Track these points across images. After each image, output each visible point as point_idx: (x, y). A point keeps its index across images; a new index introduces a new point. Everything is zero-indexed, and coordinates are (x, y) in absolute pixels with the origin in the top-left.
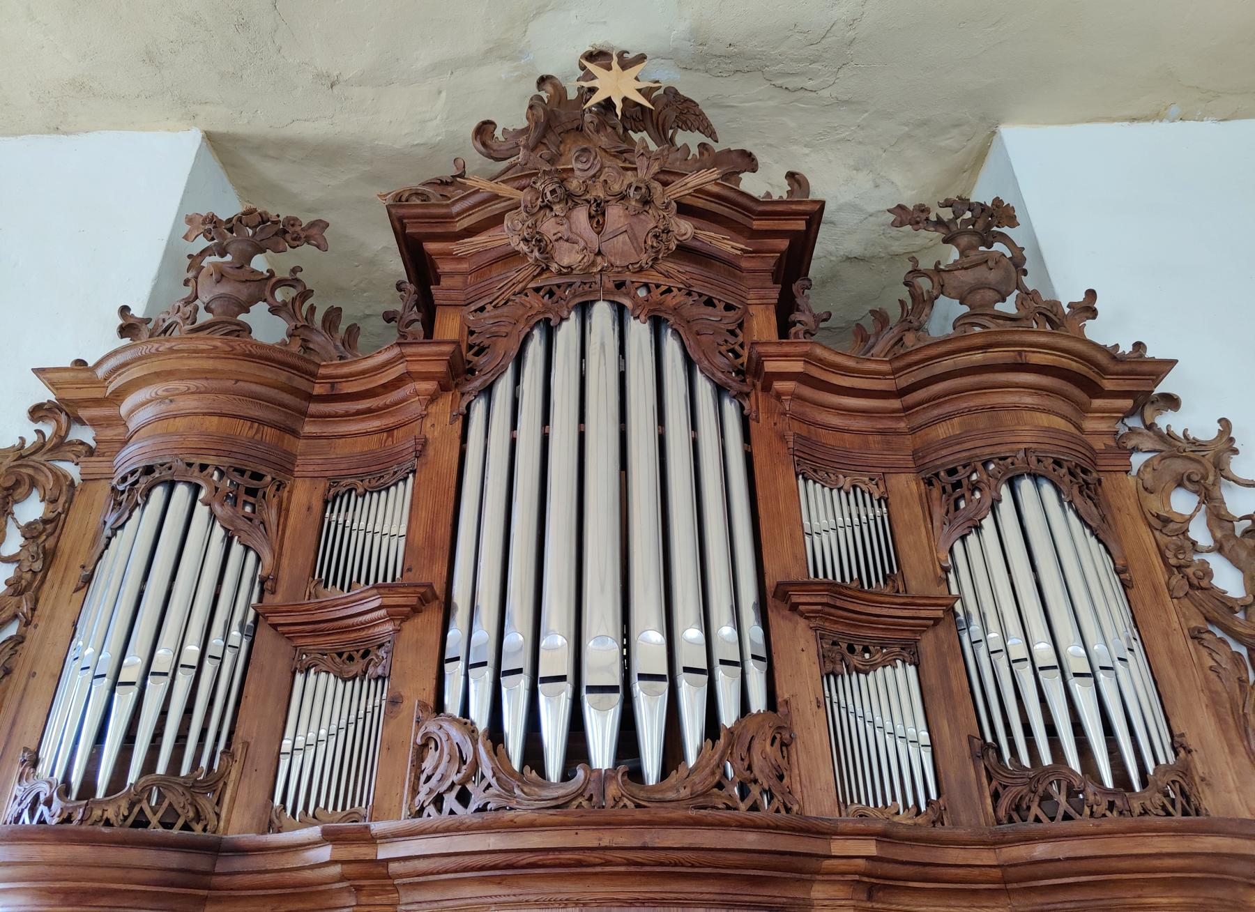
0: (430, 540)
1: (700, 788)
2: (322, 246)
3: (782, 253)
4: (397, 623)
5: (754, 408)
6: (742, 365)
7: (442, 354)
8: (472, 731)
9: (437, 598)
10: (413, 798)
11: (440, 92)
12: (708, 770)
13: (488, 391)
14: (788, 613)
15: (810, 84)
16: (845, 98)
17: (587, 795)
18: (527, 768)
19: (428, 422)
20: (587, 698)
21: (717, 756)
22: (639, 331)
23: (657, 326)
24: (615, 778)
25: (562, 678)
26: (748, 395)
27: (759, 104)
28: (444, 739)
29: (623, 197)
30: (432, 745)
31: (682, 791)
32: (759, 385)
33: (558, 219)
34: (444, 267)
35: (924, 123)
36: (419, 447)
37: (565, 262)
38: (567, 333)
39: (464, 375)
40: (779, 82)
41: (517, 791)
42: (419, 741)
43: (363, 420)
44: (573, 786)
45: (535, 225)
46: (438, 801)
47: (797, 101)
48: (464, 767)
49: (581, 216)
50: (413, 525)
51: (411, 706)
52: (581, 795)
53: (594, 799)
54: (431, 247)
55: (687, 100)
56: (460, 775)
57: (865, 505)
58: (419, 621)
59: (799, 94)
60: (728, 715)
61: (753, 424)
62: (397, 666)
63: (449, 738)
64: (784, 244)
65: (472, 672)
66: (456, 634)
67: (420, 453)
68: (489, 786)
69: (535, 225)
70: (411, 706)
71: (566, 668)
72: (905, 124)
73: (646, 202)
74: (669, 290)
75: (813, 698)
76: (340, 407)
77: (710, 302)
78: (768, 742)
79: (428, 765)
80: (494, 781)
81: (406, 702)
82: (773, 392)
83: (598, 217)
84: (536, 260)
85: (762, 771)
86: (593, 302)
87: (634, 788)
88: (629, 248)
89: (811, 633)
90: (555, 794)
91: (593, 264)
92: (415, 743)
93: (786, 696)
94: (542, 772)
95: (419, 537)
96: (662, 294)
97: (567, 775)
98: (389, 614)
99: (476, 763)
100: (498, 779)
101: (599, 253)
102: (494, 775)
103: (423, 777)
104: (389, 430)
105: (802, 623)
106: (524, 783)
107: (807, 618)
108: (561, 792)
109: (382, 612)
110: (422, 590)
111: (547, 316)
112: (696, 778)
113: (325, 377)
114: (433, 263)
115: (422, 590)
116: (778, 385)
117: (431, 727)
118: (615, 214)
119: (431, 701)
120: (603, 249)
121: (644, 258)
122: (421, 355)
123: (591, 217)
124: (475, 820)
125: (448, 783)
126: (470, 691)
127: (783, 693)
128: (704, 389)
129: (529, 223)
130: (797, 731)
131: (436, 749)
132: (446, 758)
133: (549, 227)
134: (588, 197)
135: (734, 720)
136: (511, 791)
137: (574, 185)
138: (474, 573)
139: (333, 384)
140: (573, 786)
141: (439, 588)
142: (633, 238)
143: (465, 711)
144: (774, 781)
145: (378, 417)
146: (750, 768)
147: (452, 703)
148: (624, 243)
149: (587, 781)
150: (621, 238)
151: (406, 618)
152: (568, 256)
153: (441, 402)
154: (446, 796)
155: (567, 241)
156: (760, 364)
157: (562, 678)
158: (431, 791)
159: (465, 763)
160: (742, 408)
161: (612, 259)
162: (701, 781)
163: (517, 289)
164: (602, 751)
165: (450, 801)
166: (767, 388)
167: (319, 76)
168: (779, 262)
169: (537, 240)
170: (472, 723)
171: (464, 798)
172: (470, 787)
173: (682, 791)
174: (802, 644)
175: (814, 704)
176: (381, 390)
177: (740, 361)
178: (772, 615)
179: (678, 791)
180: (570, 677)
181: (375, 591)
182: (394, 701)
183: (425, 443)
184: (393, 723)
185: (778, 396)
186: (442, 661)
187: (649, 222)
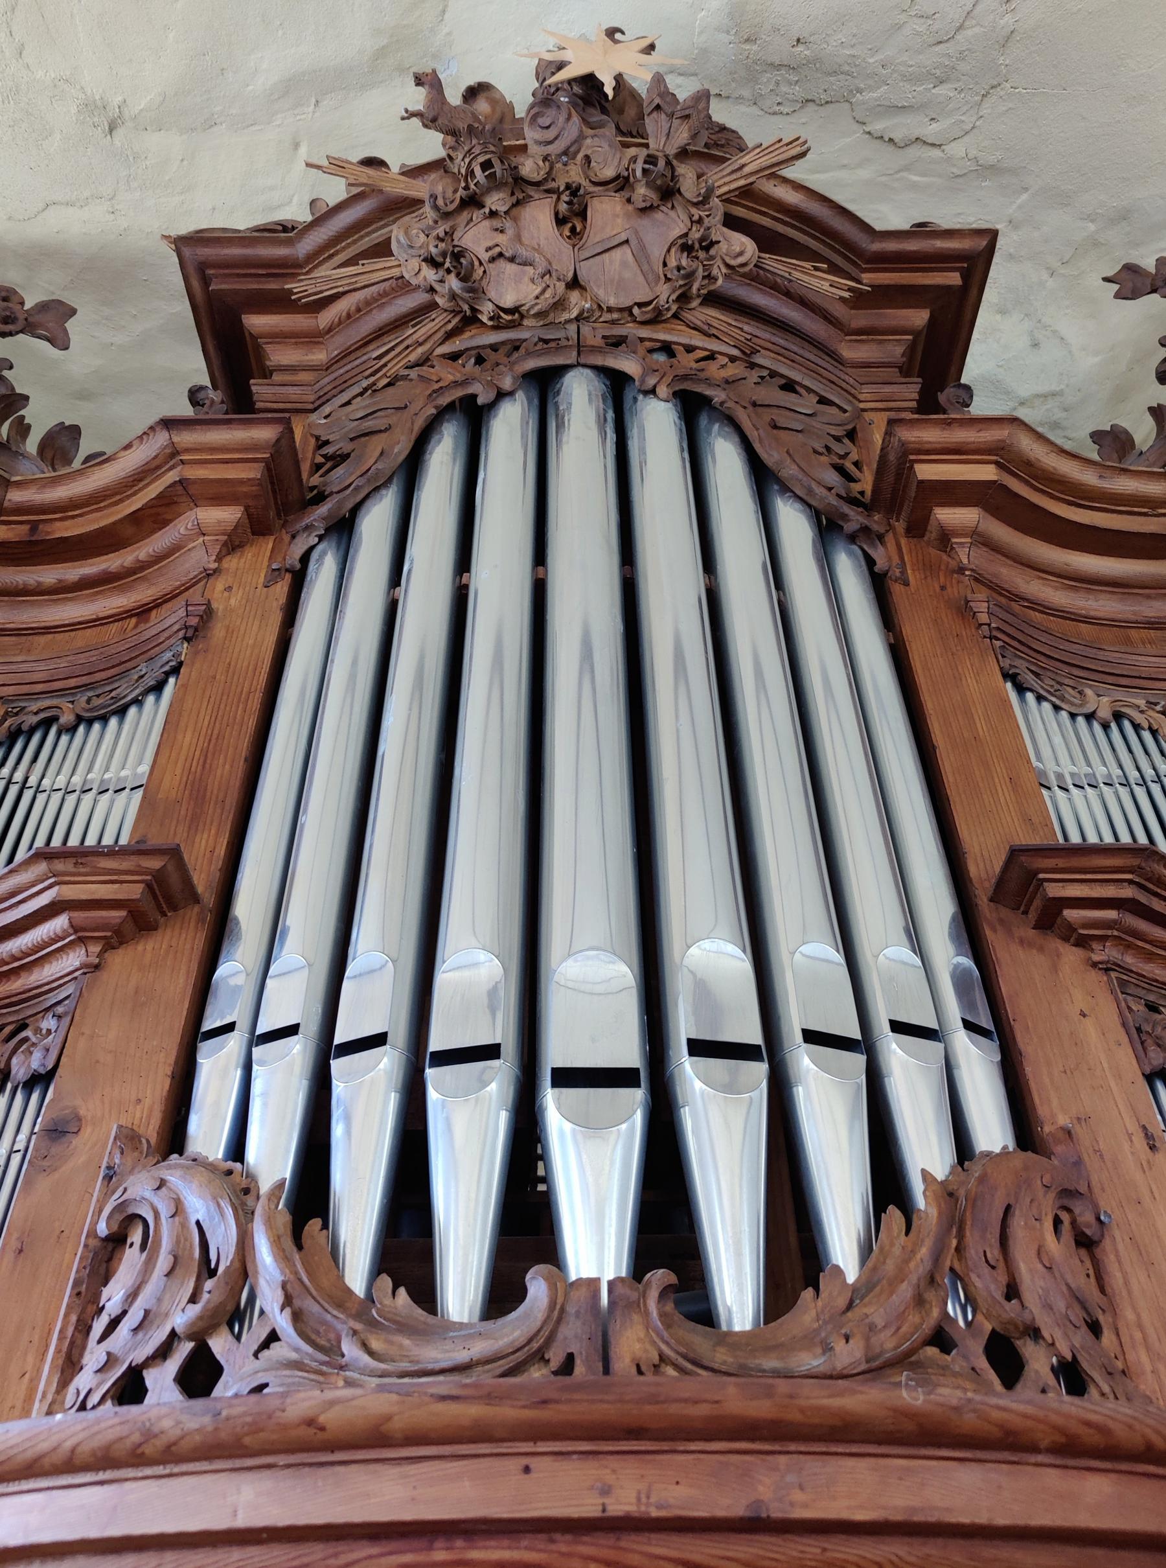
0: (197, 791)
1: (888, 1343)
2: (61, 342)
3: (916, 333)
4: (95, 949)
5: (896, 560)
6: (862, 493)
7: (255, 447)
8: (242, 1194)
9: (195, 898)
10: (64, 1384)
11: (296, 146)
12: (905, 1291)
13: (343, 529)
14: (1031, 933)
15: (931, 131)
16: (992, 159)
17: (556, 1357)
18: (386, 1281)
19: (219, 584)
20: (551, 1100)
21: (924, 1252)
22: (657, 424)
23: (693, 409)
24: (638, 1306)
25: (490, 1052)
26: (881, 538)
27: (842, 174)
28: (165, 1211)
29: (622, 183)
30: (136, 1236)
31: (840, 1346)
32: (900, 526)
33: (496, 223)
34: (279, 356)
35: (1123, 216)
36: (194, 621)
37: (508, 301)
38: (509, 428)
39: (295, 506)
40: (877, 127)
41: (350, 1349)
42: (102, 1229)
43: (93, 598)
44: (515, 1328)
45: (449, 234)
46: (130, 1389)
47: (906, 168)
48: (209, 1284)
49: (539, 218)
50: (162, 760)
51: (95, 1143)
52: (539, 1357)
53: (579, 1369)
54: (256, 322)
55: (723, 129)
56: (194, 1310)
57: (1147, 752)
58: (148, 948)
59: (915, 152)
60: (926, 1153)
61: (897, 589)
62: (78, 1047)
63: (178, 1209)
64: (919, 317)
65: (257, 1052)
66: (234, 970)
67: (193, 634)
68: (273, 1337)
69: (449, 234)
70: (95, 1143)
71: (500, 1028)
72: (1091, 218)
73: (668, 193)
74: (711, 356)
75: (1133, 1127)
76: (49, 575)
77: (789, 386)
78: (1048, 1224)
79: (113, 1296)
80: (282, 1322)
81: (87, 1132)
82: (932, 533)
83: (573, 219)
84: (453, 296)
85: (1048, 1307)
86: (559, 371)
87: (697, 1338)
88: (632, 274)
89: (1094, 976)
90: (462, 1356)
91: (560, 305)
92: (92, 1233)
93: (1063, 1120)
94: (426, 1294)
95: (172, 783)
96: (698, 361)
97: (502, 1294)
98: (75, 928)
99: (244, 1269)
100: (297, 1318)
101: (575, 283)
102: (288, 1301)
103: (99, 1326)
104: (142, 612)
105: (1071, 956)
106: (373, 1324)
107: (1083, 942)
108: (478, 1349)
109: (59, 923)
110: (155, 863)
111: (470, 390)
112: (876, 1312)
113: (20, 510)
114: (258, 350)
115: (155, 863)
116: (948, 516)
117: (139, 1188)
118: (608, 215)
119: (152, 1129)
120: (583, 277)
121: (664, 293)
122: (213, 449)
123: (560, 221)
124: (192, 1424)
125: (158, 1336)
126: (253, 1104)
127: (1053, 1112)
128: (795, 528)
129: (440, 231)
130: (1107, 1203)
131: (143, 1247)
132: (163, 1262)
133: (476, 237)
134: (553, 185)
135: (947, 1170)
136: (332, 1350)
137: (529, 168)
138: (286, 865)
139: (34, 526)
140: (515, 1328)
141: (204, 878)
142: (642, 255)
143: (237, 1148)
144: (1082, 1337)
145: (123, 590)
146: (1012, 1292)
147: (207, 1133)
148: (624, 264)
149: (557, 1314)
150: (617, 254)
151: (115, 939)
152: (511, 288)
153: (249, 554)
154: (151, 1377)
155: (512, 260)
156: (904, 469)
157: (490, 1052)
158: (111, 1360)
159: (212, 1273)
160: (870, 562)
161: (601, 293)
162: (890, 1322)
163: (413, 357)
164: (594, 1236)
165: (162, 1382)
166: (917, 528)
167: (90, 107)
168: (912, 347)
169: (454, 259)
170: (251, 1177)
171: (200, 1376)
172: (219, 1344)
173: (840, 1346)
174: (1079, 1000)
175: (1140, 1142)
176: (129, 530)
177: (856, 487)
178: (994, 938)
179: (827, 1349)
180: (510, 1049)
181: (42, 867)
182: (58, 1132)
183: (208, 614)
184: (44, 1184)
185: (945, 538)
186: (194, 1036)
187: (673, 223)
